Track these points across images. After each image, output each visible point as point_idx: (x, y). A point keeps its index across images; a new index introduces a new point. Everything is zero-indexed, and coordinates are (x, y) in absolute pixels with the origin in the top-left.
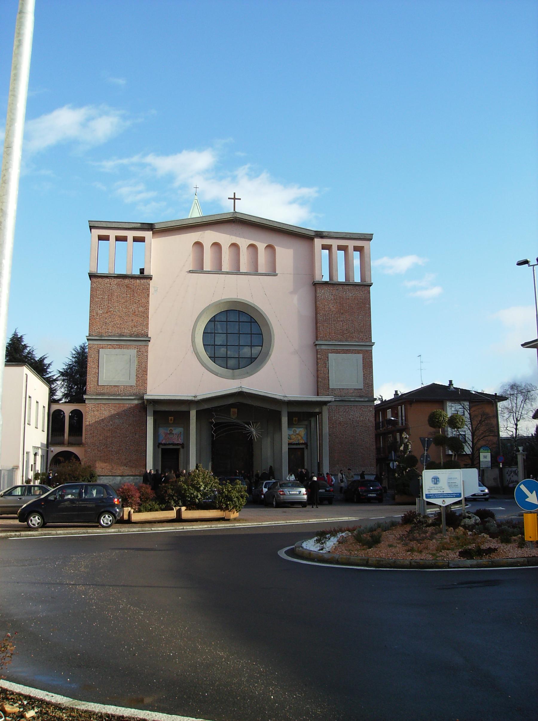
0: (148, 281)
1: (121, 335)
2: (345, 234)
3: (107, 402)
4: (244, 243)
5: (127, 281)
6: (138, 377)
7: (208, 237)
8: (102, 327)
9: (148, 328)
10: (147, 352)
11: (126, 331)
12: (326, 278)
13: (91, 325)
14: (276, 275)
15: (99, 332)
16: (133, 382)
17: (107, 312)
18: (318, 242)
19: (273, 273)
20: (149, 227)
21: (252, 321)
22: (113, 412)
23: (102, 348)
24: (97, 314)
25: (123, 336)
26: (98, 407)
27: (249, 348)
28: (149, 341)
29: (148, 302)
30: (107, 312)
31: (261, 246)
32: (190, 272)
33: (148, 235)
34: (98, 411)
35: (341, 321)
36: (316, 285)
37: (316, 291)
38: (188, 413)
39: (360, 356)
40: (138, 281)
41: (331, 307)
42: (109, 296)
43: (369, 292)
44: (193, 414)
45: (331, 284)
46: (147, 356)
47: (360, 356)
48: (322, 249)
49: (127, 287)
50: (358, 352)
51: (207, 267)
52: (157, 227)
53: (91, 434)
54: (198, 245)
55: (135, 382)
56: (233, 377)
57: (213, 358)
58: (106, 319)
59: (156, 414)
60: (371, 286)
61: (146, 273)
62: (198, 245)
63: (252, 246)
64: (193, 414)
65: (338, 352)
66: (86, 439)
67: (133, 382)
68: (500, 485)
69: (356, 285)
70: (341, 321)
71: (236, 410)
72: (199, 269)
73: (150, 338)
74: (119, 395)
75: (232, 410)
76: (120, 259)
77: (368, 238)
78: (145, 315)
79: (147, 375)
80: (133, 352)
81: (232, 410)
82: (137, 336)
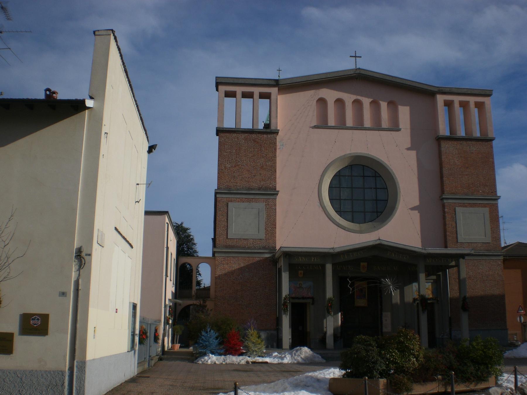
0: (275, 135)
1: (249, 189)
2: (449, 89)
3: (236, 255)
4: (348, 98)
5: (254, 136)
6: (267, 230)
7: (330, 95)
8: (230, 181)
9: (275, 181)
10: (275, 205)
11: (254, 184)
12: (447, 133)
13: (219, 178)
14: (399, 130)
15: (228, 186)
16: (262, 235)
17: (235, 166)
18: (440, 99)
19: (395, 127)
20: (276, 83)
21: (376, 175)
22: (242, 265)
23: (231, 201)
24: (225, 167)
25: (251, 189)
26: (228, 260)
27: (341, 198)
28: (277, 194)
29: (275, 156)
30: (235, 166)
31: (366, 102)
32: (315, 127)
33: (274, 91)
34: (228, 264)
35: (467, 175)
36: (440, 139)
37: (439, 146)
38: (323, 267)
39: (487, 209)
40: (265, 136)
41: (456, 162)
42: (236, 150)
43: (492, 147)
44: (329, 268)
45: (452, 138)
46: (276, 209)
47: (487, 209)
48: (225, 97)
49: (254, 141)
50: (484, 206)
51: (349, 122)
52: (281, 83)
53: (221, 287)
54: (322, 101)
55: (265, 235)
56: (361, 232)
57: (339, 212)
58: (234, 172)
59: (293, 269)
60: (493, 140)
61: (273, 127)
62: (322, 101)
63: (340, 102)
64: (329, 268)
65: (464, 206)
66: (215, 292)
67: (262, 235)
68: (399, 302)
69: (477, 140)
70: (467, 175)
71: (365, 264)
72: (322, 124)
73: (278, 191)
74: (249, 248)
75: (362, 264)
76: (247, 114)
77: (487, 94)
78: (273, 170)
79: (276, 228)
80: (261, 205)
81: (362, 264)
82: (259, 189)
